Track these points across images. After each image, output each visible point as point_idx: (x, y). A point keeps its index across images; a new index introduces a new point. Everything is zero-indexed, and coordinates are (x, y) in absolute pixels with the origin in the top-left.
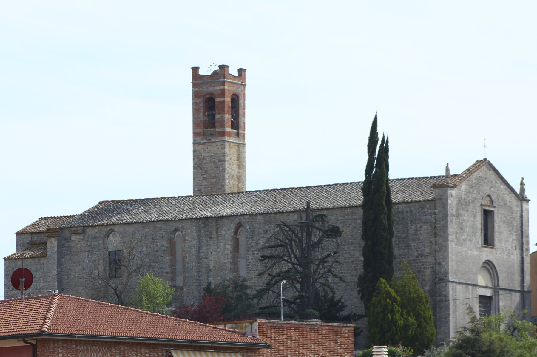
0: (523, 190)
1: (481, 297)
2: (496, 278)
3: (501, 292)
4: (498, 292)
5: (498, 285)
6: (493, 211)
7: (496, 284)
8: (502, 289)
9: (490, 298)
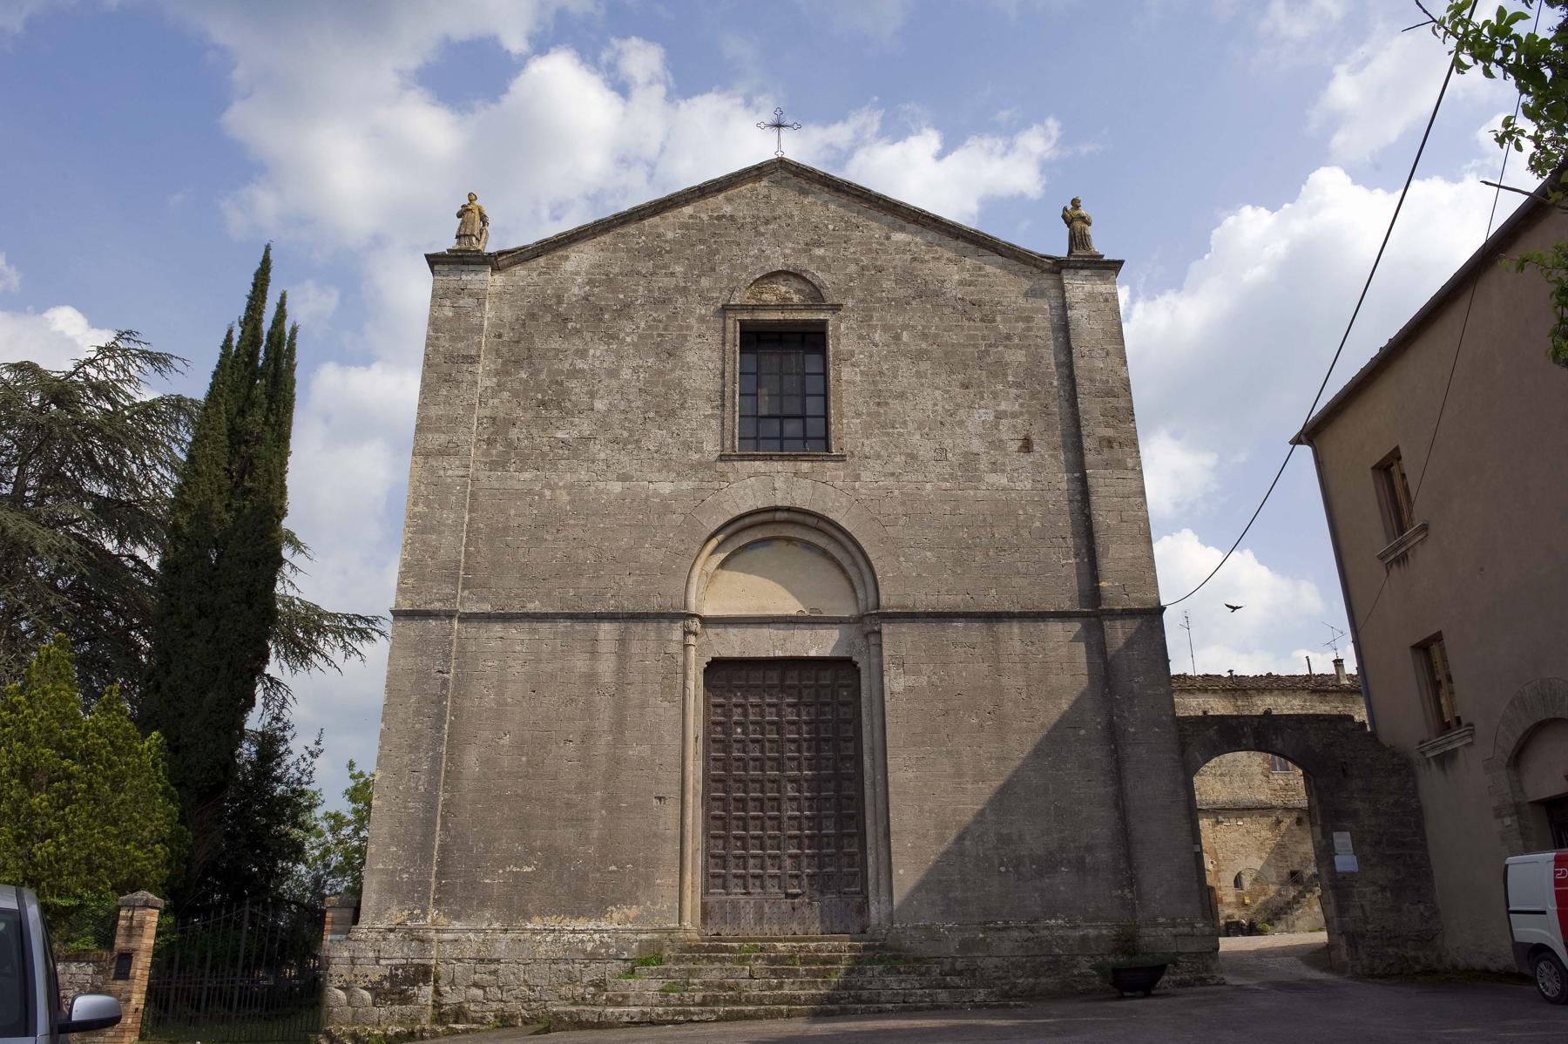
0: (1078, 240)
1: (716, 667)
2: (852, 549)
3: (896, 640)
4: (879, 632)
5: (878, 606)
6: (824, 323)
7: (872, 600)
8: (911, 616)
9: (841, 666)
